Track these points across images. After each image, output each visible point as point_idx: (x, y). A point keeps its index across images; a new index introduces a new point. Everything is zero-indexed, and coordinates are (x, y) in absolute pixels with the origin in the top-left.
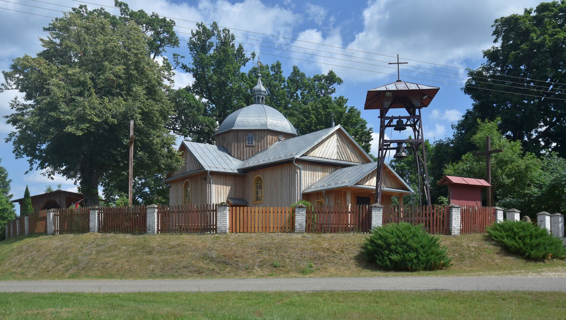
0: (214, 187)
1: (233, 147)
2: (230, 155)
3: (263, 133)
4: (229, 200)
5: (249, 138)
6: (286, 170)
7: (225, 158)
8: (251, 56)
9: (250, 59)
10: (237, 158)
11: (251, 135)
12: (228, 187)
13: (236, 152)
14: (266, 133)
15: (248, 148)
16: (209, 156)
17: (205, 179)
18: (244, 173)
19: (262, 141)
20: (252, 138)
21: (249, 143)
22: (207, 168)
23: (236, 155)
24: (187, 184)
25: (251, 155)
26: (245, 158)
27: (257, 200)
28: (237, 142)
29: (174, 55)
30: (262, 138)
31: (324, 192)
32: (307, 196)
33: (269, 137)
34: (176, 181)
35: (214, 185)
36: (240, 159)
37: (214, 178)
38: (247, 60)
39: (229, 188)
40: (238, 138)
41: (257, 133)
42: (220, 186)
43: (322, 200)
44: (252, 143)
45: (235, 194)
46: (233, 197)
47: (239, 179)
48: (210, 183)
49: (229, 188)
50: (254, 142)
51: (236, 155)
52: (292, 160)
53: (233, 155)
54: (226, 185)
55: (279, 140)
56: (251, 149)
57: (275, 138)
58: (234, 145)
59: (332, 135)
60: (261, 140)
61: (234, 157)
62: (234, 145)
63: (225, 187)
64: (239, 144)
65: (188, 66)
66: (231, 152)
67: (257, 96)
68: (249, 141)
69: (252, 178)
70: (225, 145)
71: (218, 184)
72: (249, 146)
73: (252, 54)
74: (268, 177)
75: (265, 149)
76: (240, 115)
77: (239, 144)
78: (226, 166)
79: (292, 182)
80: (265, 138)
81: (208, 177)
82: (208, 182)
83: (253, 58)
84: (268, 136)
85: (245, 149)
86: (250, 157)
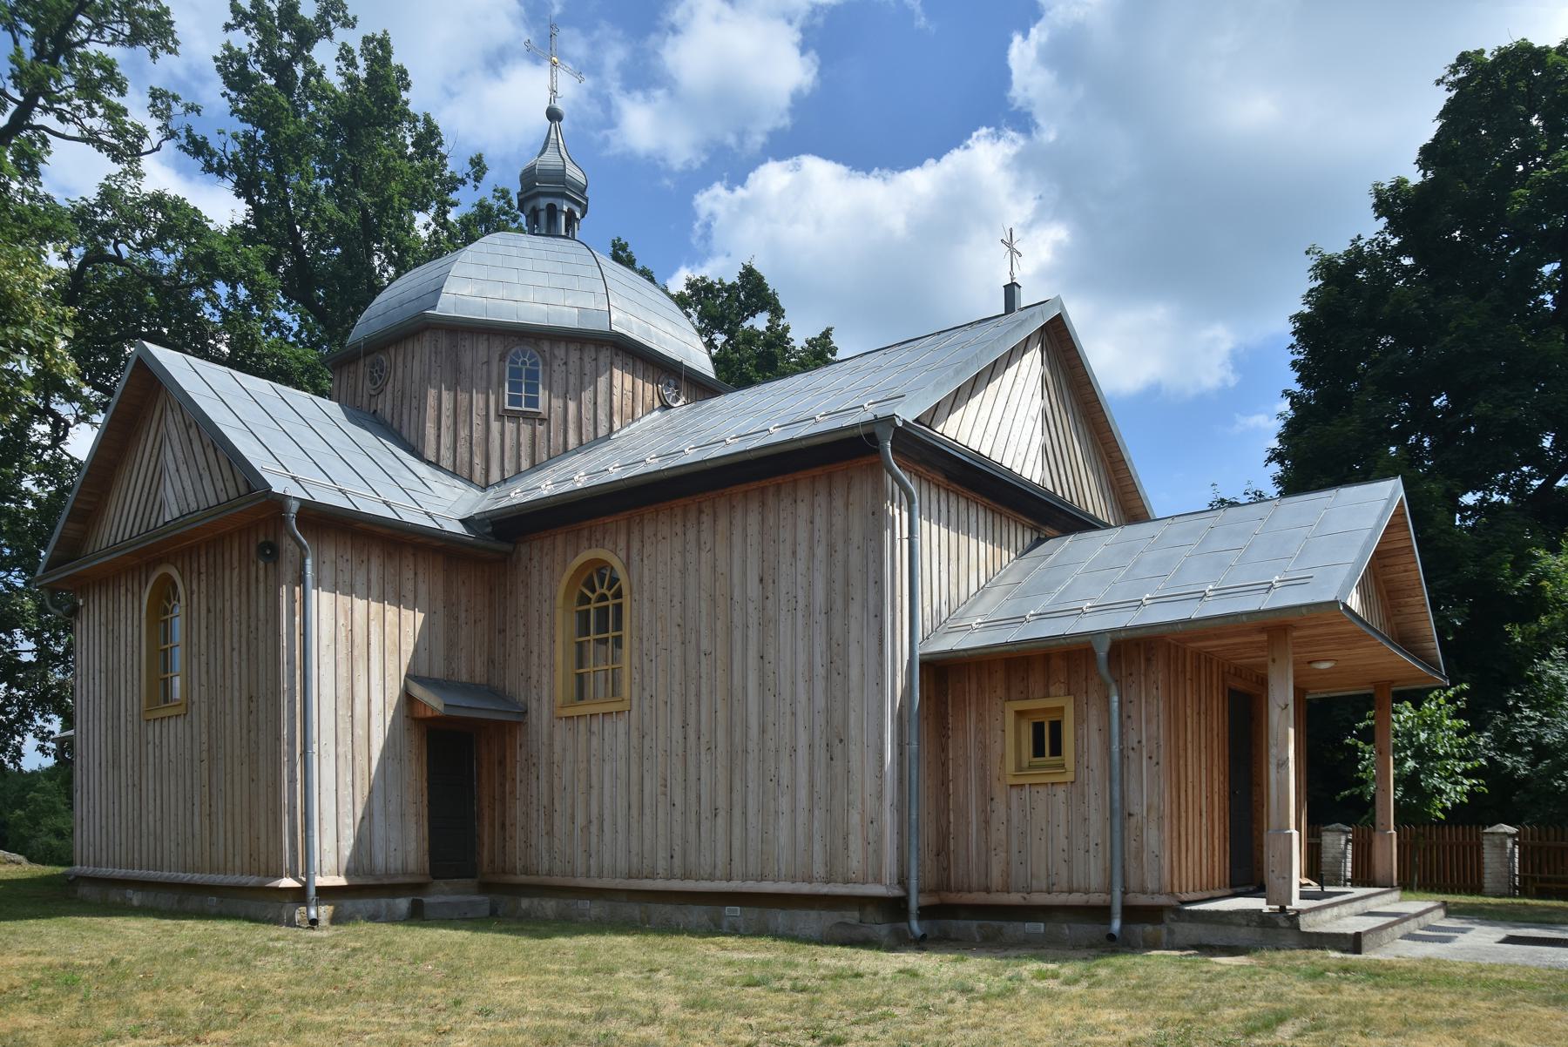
0: (325, 606)
1: (431, 413)
2: (420, 457)
3: (590, 352)
4: (418, 691)
5: (515, 373)
6: (802, 520)
7: (388, 461)
8: (468, 169)
9: (463, 182)
10: (454, 474)
11: (525, 356)
12: (407, 614)
13: (446, 440)
14: (604, 356)
15: (510, 426)
16: (295, 441)
17: (271, 552)
18: (505, 539)
19: (587, 395)
20: (532, 375)
21: (515, 400)
22: (278, 485)
23: (446, 454)
24: (164, 595)
25: (525, 465)
26: (495, 476)
27: (581, 695)
28: (454, 387)
29: (156, 95)
30: (585, 380)
31: (1102, 652)
32: (944, 676)
33: (622, 380)
34: (107, 579)
35: (326, 598)
36: (470, 481)
37: (329, 554)
38: (454, 183)
39: (412, 621)
40: (457, 369)
41: (560, 351)
42: (360, 604)
43: (1068, 704)
44: (533, 402)
45: (448, 659)
46: (439, 672)
47: (474, 568)
48: (301, 580)
49: (412, 621)
50: (543, 395)
51: (446, 454)
52: (872, 437)
53: (430, 454)
54: (399, 601)
55: (666, 407)
56: (526, 429)
57: (647, 390)
58: (438, 401)
59: (1024, 347)
60: (582, 389)
61: (436, 465)
62: (438, 401)
63: (391, 611)
64: (463, 398)
65: (215, 143)
66: (422, 436)
67: (543, 203)
68: (515, 387)
69: (551, 577)
70: (385, 405)
71: (351, 591)
72: (515, 416)
73: (472, 162)
74: (660, 572)
75: (597, 440)
76: (456, 270)
77: (463, 398)
78: (396, 497)
79: (860, 585)
80: (602, 382)
81: (287, 544)
82: (288, 571)
83: (478, 179)
84: (617, 373)
85: (495, 426)
86: (519, 472)
